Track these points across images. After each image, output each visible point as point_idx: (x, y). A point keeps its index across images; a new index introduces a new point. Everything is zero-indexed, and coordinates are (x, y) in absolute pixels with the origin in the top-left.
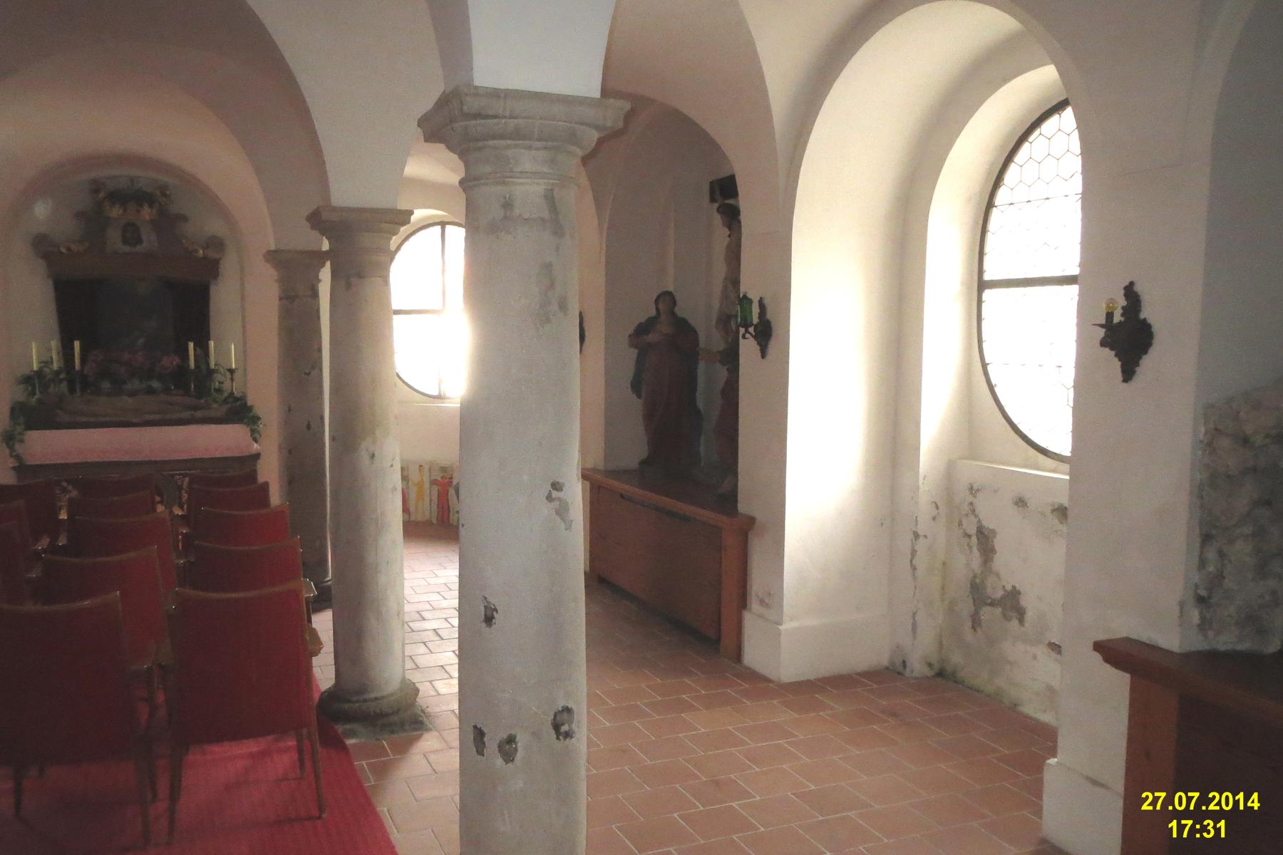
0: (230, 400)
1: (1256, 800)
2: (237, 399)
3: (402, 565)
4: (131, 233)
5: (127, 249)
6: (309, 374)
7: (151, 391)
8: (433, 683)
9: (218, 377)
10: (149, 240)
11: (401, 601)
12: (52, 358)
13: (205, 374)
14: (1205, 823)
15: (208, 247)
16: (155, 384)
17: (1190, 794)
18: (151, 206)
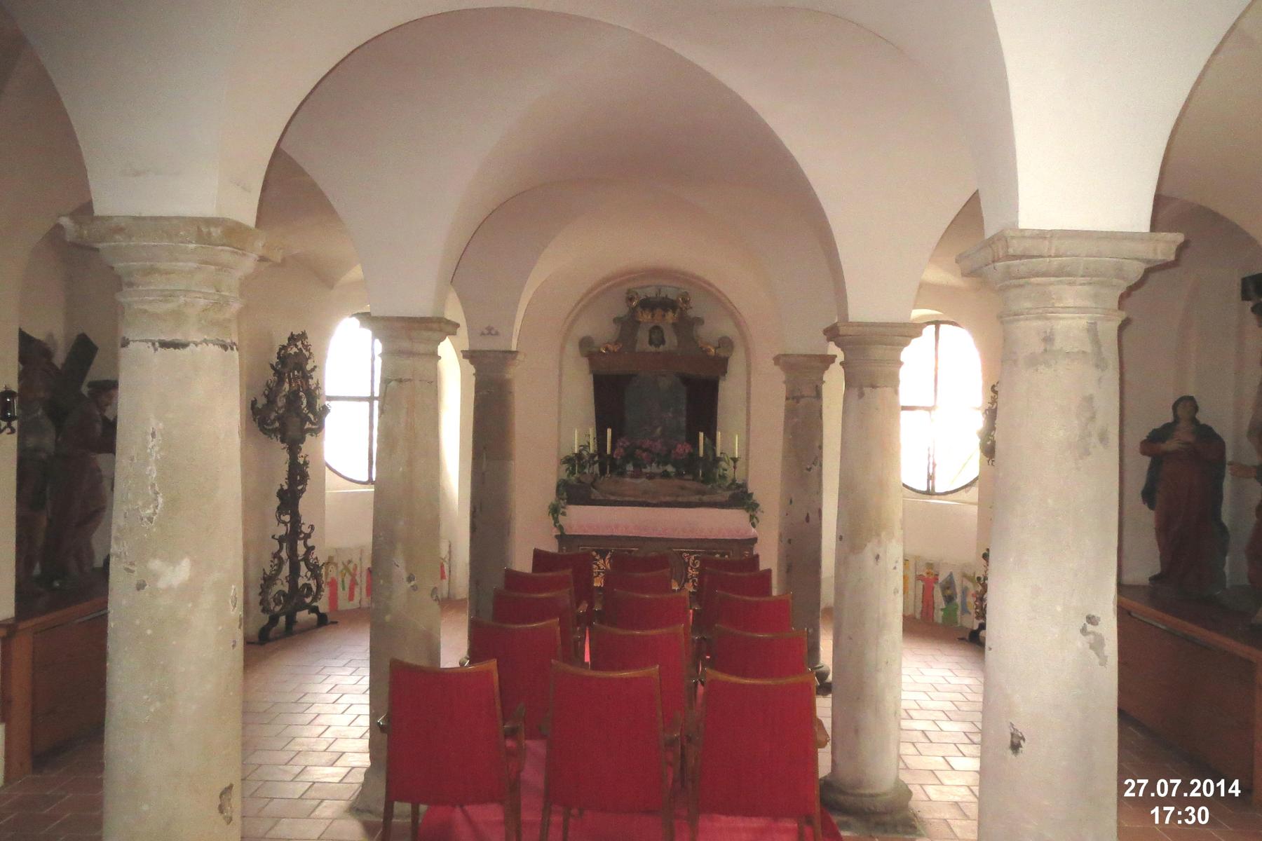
0: (733, 487)
1: (1237, 787)
2: (739, 486)
3: (900, 664)
4: (657, 335)
5: (652, 349)
6: (809, 470)
7: (666, 475)
8: (924, 787)
9: (723, 464)
10: (671, 341)
11: (898, 701)
12: (589, 443)
13: (713, 461)
14: (1187, 809)
15: (719, 347)
16: (670, 469)
17: (1172, 781)
18: (674, 312)
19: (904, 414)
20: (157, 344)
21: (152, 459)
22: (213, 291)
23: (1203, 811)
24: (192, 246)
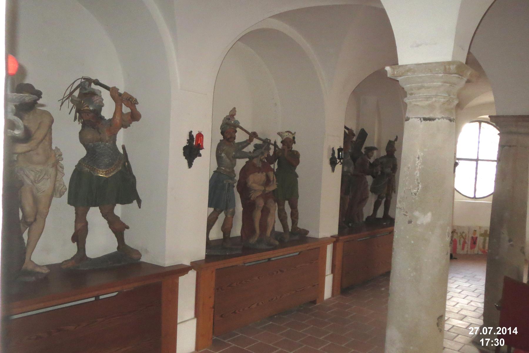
1: (516, 331)
14: (495, 340)
17: (489, 328)
19: (496, 159)
20: (422, 119)
21: (418, 168)
22: (447, 95)
23: (502, 341)
24: (441, 75)
